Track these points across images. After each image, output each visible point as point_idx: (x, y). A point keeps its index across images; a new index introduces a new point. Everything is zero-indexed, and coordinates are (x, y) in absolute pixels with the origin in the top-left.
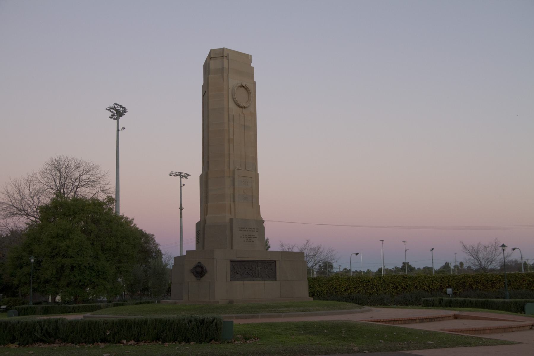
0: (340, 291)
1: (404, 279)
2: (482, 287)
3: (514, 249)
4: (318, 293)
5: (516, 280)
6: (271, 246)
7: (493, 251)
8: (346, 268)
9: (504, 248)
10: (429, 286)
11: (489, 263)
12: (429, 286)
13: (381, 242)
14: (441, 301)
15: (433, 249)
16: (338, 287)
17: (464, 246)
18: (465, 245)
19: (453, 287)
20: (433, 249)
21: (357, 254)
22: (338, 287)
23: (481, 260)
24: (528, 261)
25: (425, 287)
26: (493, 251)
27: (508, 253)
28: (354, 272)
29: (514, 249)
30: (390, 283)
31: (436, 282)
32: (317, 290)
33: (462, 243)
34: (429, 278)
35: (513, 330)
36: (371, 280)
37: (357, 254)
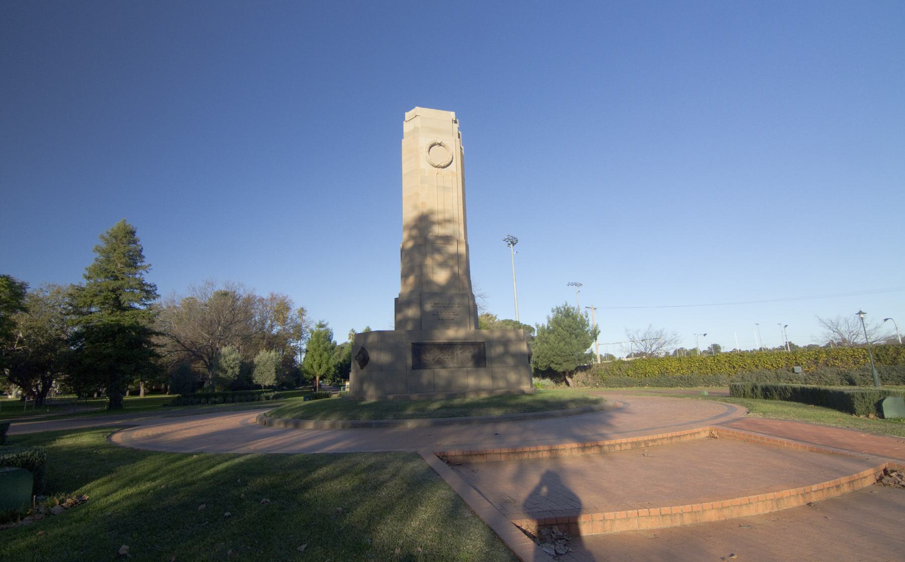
0: (672, 371)
1: (740, 357)
2: (840, 364)
3: (886, 320)
4: (650, 374)
5: (886, 354)
6: (601, 331)
7: (857, 322)
8: (721, 347)
9: (862, 316)
10: (772, 365)
11: (855, 336)
12: (772, 365)
13: (779, 325)
14: (742, 402)
15: (786, 326)
16: (670, 367)
17: (821, 320)
18: (821, 318)
19: (802, 364)
20: (786, 326)
21: (705, 335)
22: (670, 367)
23: (843, 334)
24: (638, 335)
25: (768, 366)
26: (857, 322)
27: (877, 324)
28: (602, 358)
29: (886, 320)
30: (725, 362)
31: (780, 359)
32: (647, 371)
33: (818, 317)
34: (771, 356)
35: (894, 327)
36: (704, 359)
37: (705, 335)
